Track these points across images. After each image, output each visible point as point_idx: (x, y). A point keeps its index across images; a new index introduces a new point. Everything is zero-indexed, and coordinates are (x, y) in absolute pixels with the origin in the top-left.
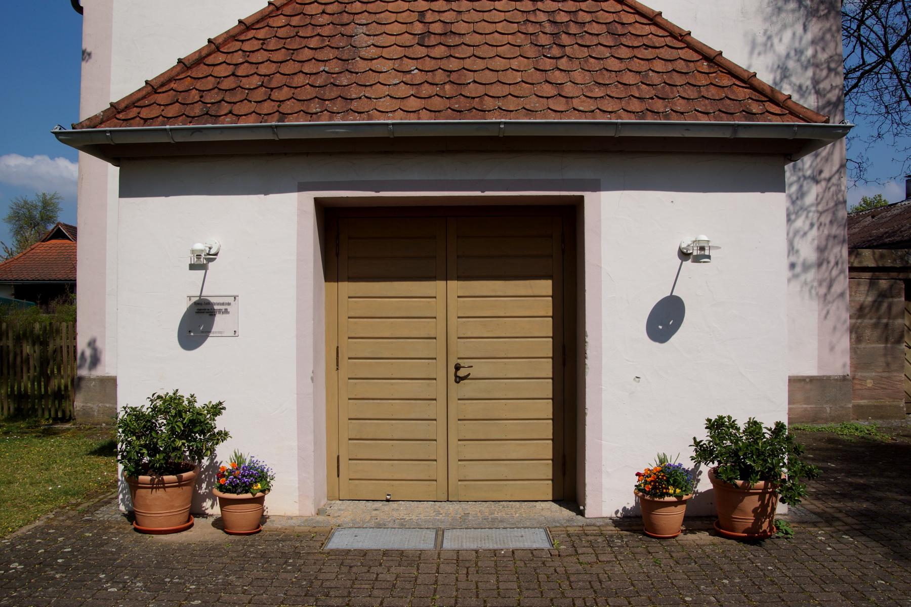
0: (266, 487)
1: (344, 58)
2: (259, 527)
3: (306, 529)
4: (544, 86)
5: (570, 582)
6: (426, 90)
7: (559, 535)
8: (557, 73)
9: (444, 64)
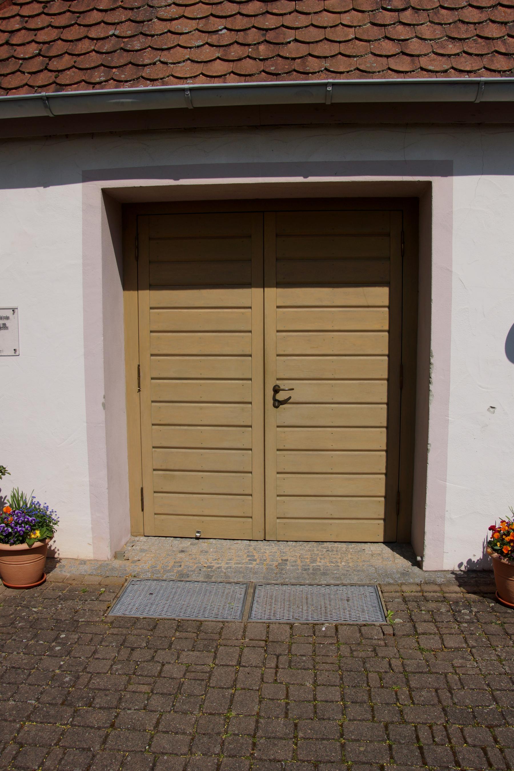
0: (47, 534)
1: (138, 19)
2: (42, 576)
3: (97, 579)
4: (383, 44)
5: (410, 690)
6: (235, 52)
7: (394, 598)
8: (400, 28)
9: (259, 22)
